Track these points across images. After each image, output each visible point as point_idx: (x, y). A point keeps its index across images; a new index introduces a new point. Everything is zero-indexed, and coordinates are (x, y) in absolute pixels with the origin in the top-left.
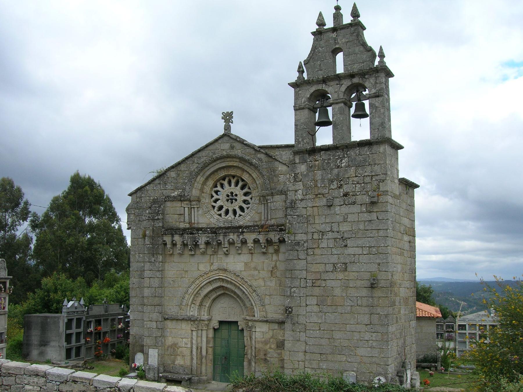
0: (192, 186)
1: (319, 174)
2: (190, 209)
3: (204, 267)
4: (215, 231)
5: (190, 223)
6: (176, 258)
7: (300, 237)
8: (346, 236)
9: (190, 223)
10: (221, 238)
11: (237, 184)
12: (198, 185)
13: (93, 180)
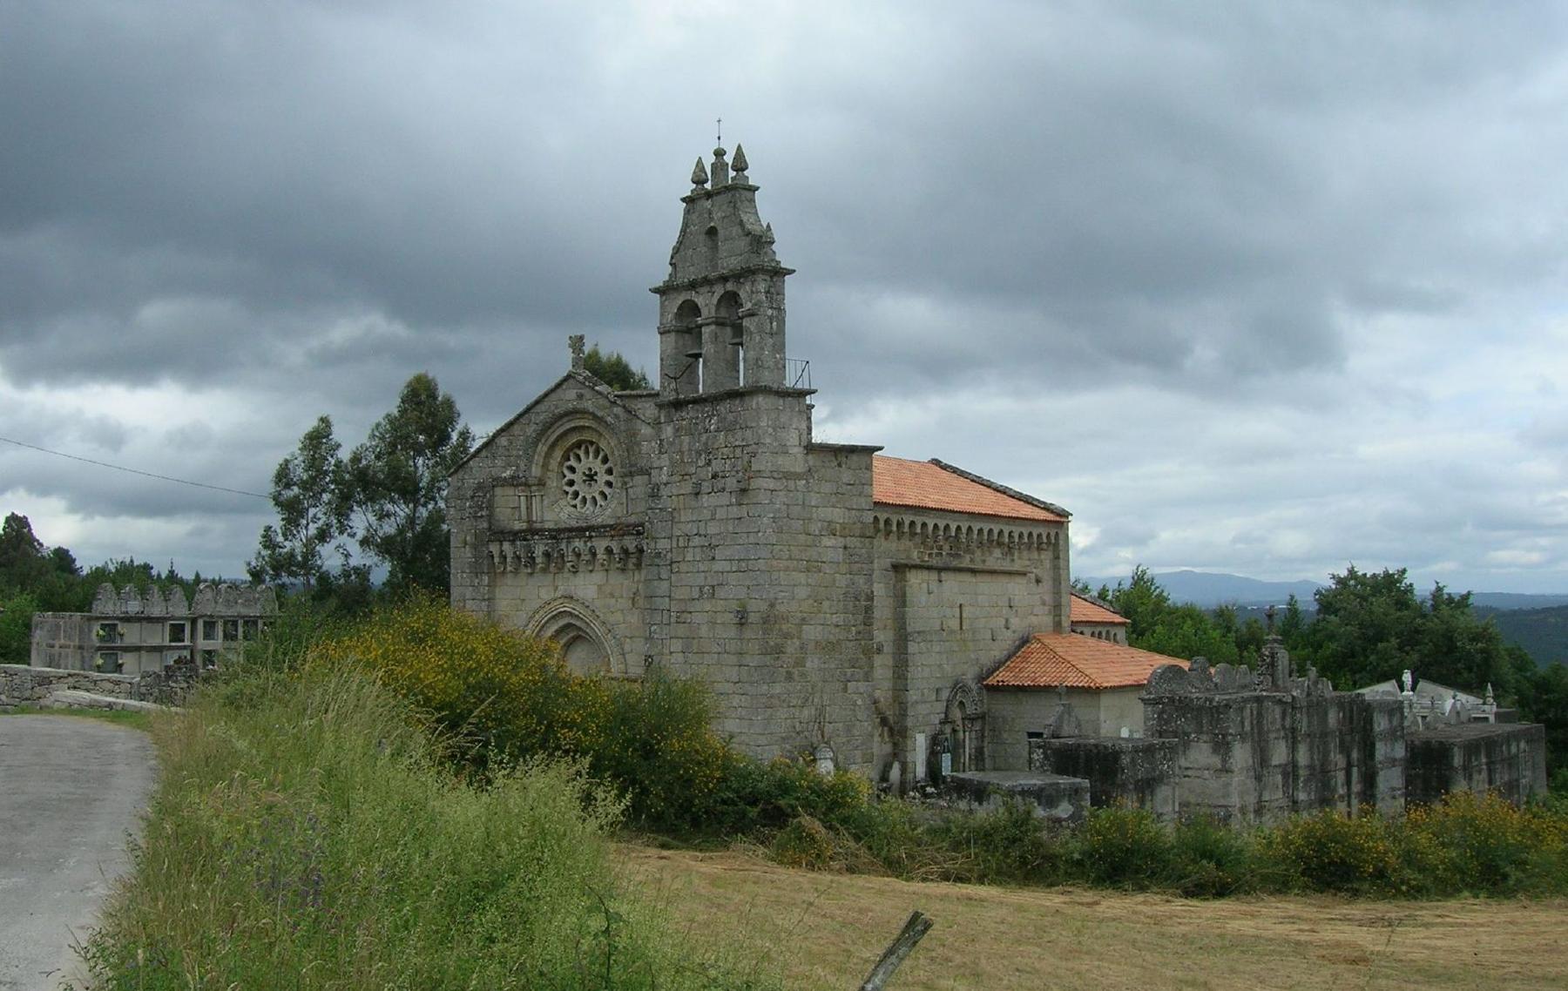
0: (530, 461)
1: (686, 439)
2: (529, 499)
3: (546, 594)
4: (556, 534)
5: (529, 521)
6: (509, 579)
7: (663, 544)
8: (714, 542)
9: (529, 521)
10: (563, 546)
11: (596, 457)
12: (538, 459)
13: (626, 367)
